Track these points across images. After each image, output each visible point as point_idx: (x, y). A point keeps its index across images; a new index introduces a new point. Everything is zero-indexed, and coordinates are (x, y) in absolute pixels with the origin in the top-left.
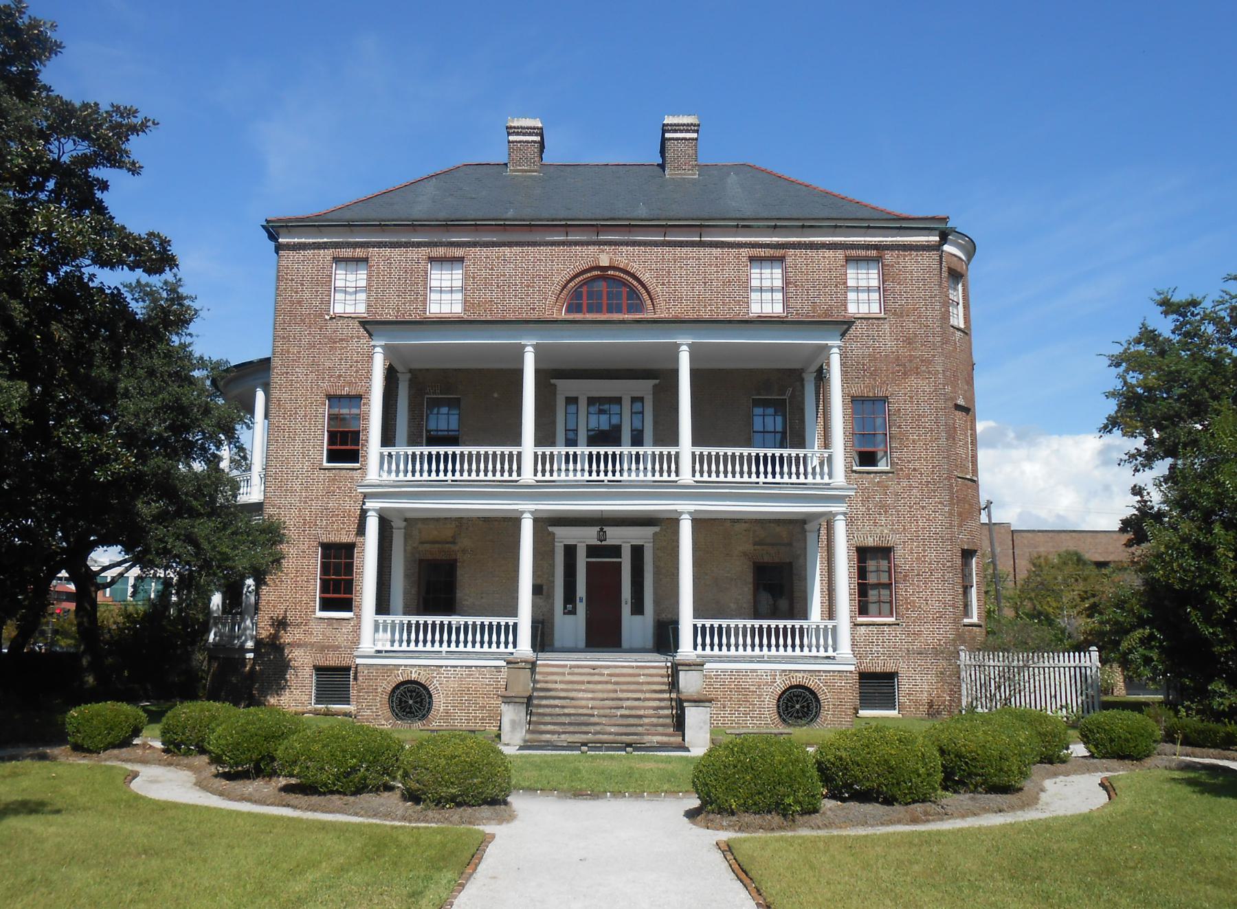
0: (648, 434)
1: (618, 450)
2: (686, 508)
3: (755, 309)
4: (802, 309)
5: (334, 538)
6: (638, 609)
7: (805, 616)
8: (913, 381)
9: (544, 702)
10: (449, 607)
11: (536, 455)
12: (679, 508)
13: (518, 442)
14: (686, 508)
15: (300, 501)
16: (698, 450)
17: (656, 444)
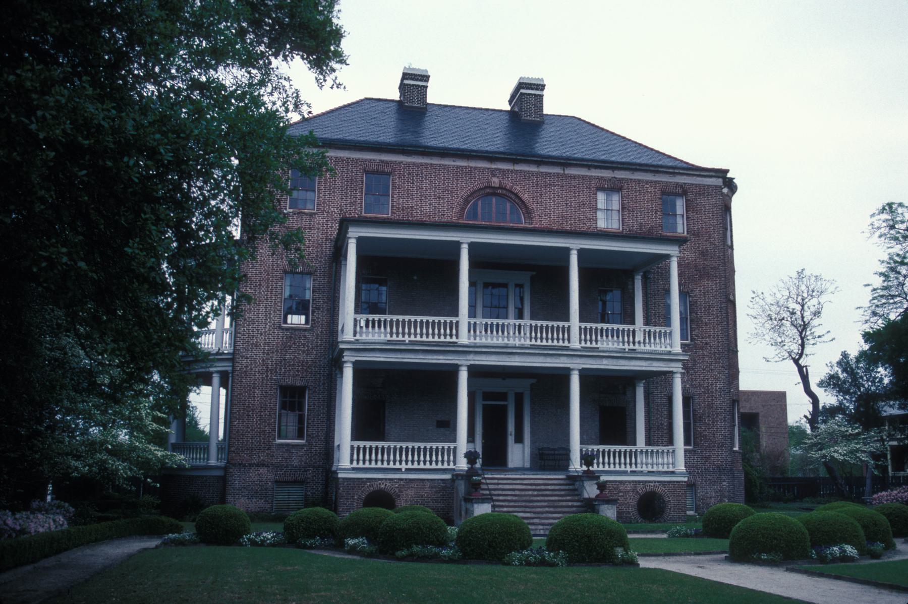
0: (527, 312)
1: (506, 322)
2: (576, 365)
3: (602, 224)
4: (634, 224)
5: (289, 382)
6: (519, 439)
7: (635, 444)
8: (706, 282)
9: (563, 493)
10: (380, 436)
11: (469, 323)
12: (571, 366)
13: (567, 319)
14: (576, 365)
15: (264, 353)
16: (583, 325)
17: (532, 318)
